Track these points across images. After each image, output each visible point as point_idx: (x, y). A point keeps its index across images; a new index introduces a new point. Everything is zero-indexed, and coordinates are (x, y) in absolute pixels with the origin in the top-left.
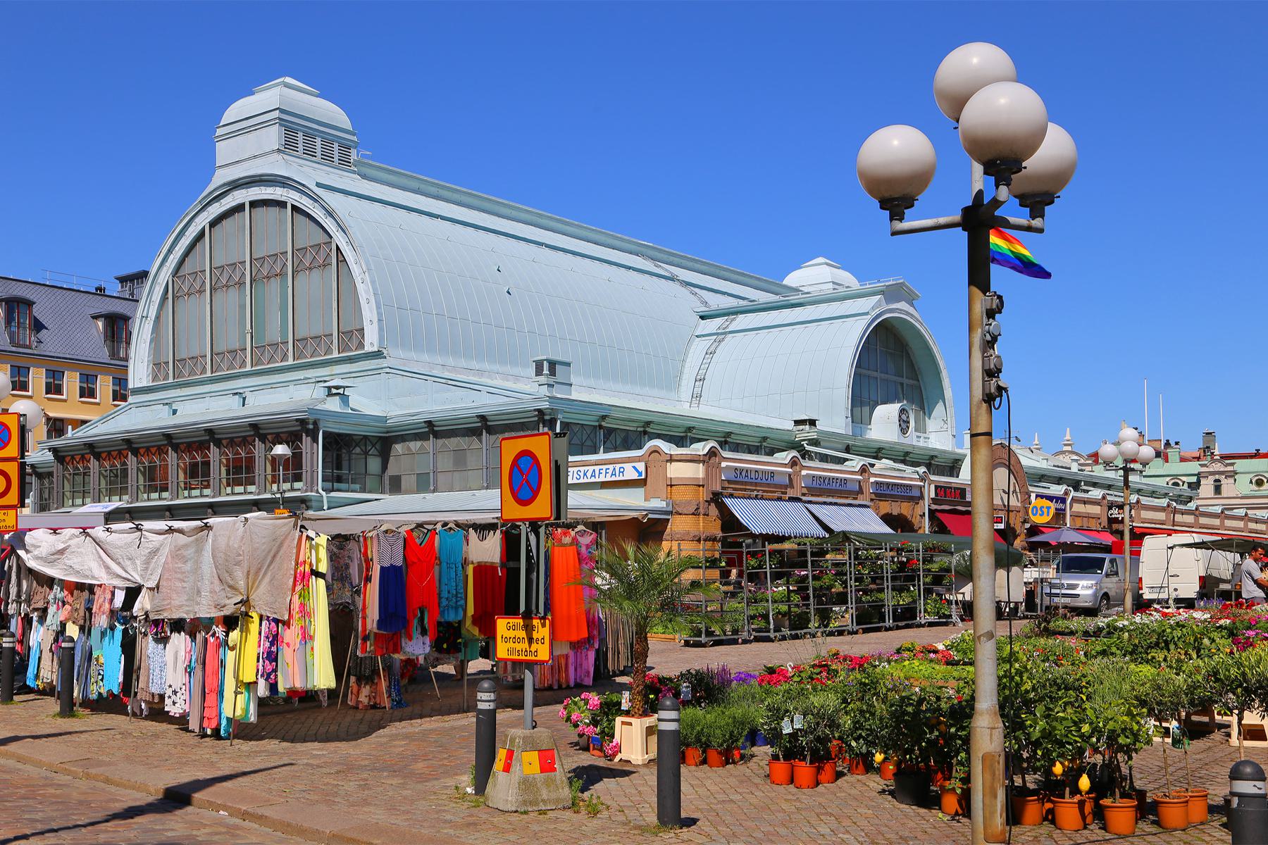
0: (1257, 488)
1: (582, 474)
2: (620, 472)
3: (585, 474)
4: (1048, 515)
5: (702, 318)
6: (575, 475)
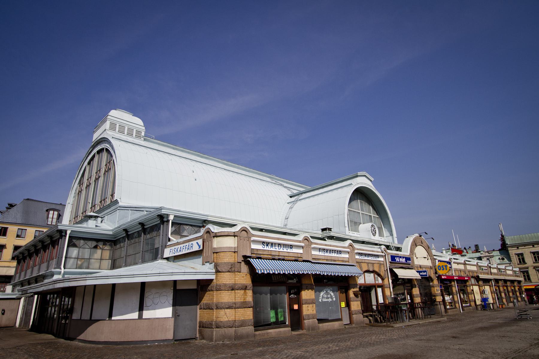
0: (502, 261)
1: (176, 250)
2: (191, 247)
4: (446, 269)
5: (291, 197)
6: (174, 251)
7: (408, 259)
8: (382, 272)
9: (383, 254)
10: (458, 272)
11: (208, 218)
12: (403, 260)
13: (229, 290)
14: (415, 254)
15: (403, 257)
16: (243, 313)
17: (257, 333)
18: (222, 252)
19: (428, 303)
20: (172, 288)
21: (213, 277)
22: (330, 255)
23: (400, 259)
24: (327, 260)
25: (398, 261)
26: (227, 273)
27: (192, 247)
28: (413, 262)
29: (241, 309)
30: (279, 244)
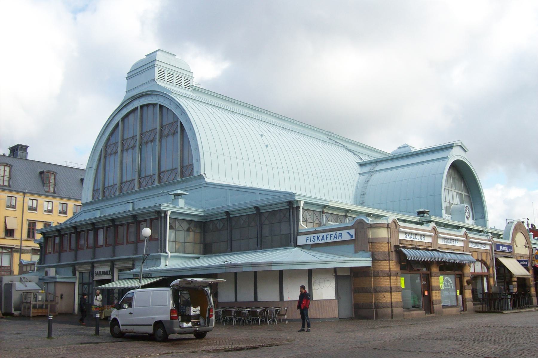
1: (316, 238)
2: (339, 236)
3: (318, 238)
6: (312, 239)
7: (510, 247)
8: (488, 261)
9: (490, 243)
10: (477, 254)
11: (328, 204)
12: (506, 249)
13: (386, 276)
14: (516, 242)
15: (506, 246)
16: (396, 296)
17: (405, 313)
18: (378, 242)
19: (158, 354)
20: (334, 274)
21: (369, 264)
22: (450, 244)
23: (504, 247)
24: (448, 249)
25: (501, 250)
26: (383, 261)
27: (341, 236)
28: (514, 251)
29: (395, 293)
30: (416, 234)
